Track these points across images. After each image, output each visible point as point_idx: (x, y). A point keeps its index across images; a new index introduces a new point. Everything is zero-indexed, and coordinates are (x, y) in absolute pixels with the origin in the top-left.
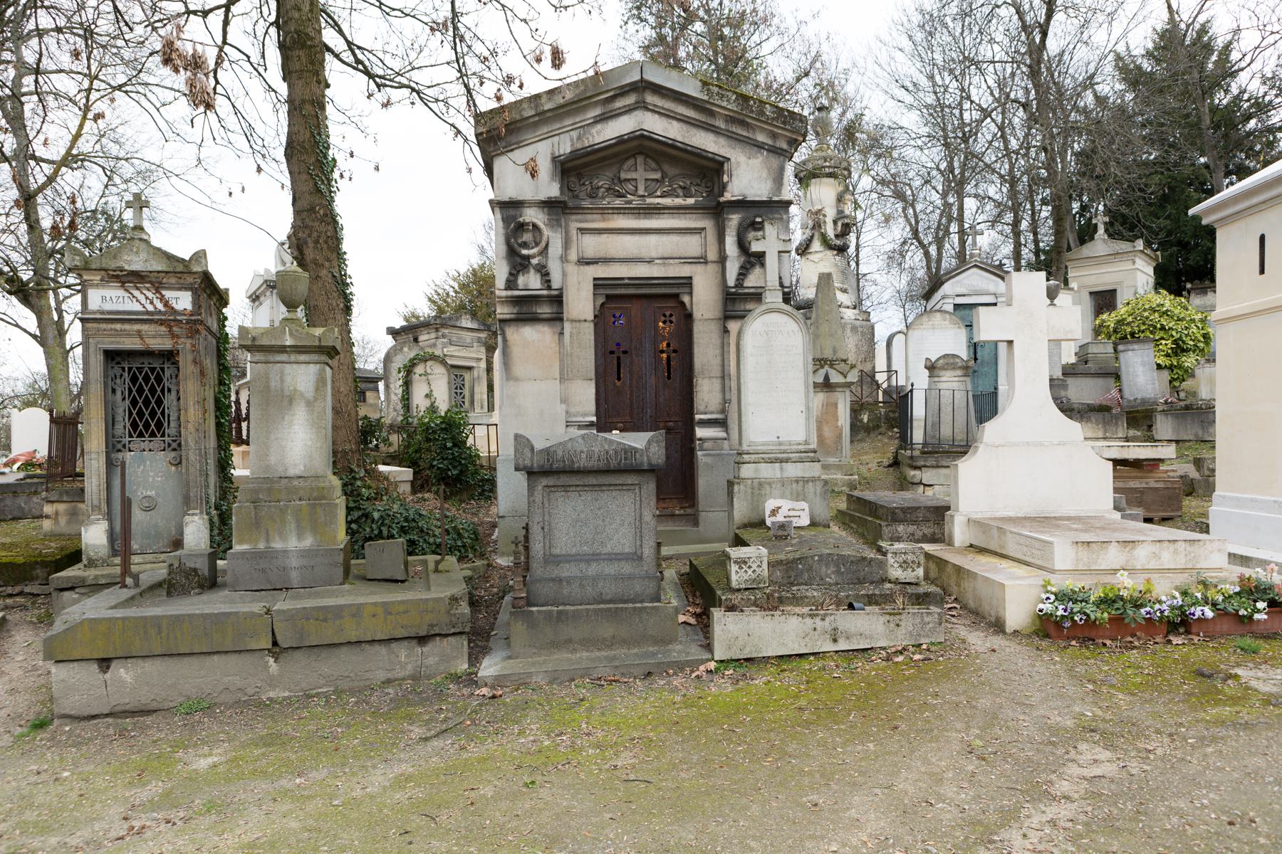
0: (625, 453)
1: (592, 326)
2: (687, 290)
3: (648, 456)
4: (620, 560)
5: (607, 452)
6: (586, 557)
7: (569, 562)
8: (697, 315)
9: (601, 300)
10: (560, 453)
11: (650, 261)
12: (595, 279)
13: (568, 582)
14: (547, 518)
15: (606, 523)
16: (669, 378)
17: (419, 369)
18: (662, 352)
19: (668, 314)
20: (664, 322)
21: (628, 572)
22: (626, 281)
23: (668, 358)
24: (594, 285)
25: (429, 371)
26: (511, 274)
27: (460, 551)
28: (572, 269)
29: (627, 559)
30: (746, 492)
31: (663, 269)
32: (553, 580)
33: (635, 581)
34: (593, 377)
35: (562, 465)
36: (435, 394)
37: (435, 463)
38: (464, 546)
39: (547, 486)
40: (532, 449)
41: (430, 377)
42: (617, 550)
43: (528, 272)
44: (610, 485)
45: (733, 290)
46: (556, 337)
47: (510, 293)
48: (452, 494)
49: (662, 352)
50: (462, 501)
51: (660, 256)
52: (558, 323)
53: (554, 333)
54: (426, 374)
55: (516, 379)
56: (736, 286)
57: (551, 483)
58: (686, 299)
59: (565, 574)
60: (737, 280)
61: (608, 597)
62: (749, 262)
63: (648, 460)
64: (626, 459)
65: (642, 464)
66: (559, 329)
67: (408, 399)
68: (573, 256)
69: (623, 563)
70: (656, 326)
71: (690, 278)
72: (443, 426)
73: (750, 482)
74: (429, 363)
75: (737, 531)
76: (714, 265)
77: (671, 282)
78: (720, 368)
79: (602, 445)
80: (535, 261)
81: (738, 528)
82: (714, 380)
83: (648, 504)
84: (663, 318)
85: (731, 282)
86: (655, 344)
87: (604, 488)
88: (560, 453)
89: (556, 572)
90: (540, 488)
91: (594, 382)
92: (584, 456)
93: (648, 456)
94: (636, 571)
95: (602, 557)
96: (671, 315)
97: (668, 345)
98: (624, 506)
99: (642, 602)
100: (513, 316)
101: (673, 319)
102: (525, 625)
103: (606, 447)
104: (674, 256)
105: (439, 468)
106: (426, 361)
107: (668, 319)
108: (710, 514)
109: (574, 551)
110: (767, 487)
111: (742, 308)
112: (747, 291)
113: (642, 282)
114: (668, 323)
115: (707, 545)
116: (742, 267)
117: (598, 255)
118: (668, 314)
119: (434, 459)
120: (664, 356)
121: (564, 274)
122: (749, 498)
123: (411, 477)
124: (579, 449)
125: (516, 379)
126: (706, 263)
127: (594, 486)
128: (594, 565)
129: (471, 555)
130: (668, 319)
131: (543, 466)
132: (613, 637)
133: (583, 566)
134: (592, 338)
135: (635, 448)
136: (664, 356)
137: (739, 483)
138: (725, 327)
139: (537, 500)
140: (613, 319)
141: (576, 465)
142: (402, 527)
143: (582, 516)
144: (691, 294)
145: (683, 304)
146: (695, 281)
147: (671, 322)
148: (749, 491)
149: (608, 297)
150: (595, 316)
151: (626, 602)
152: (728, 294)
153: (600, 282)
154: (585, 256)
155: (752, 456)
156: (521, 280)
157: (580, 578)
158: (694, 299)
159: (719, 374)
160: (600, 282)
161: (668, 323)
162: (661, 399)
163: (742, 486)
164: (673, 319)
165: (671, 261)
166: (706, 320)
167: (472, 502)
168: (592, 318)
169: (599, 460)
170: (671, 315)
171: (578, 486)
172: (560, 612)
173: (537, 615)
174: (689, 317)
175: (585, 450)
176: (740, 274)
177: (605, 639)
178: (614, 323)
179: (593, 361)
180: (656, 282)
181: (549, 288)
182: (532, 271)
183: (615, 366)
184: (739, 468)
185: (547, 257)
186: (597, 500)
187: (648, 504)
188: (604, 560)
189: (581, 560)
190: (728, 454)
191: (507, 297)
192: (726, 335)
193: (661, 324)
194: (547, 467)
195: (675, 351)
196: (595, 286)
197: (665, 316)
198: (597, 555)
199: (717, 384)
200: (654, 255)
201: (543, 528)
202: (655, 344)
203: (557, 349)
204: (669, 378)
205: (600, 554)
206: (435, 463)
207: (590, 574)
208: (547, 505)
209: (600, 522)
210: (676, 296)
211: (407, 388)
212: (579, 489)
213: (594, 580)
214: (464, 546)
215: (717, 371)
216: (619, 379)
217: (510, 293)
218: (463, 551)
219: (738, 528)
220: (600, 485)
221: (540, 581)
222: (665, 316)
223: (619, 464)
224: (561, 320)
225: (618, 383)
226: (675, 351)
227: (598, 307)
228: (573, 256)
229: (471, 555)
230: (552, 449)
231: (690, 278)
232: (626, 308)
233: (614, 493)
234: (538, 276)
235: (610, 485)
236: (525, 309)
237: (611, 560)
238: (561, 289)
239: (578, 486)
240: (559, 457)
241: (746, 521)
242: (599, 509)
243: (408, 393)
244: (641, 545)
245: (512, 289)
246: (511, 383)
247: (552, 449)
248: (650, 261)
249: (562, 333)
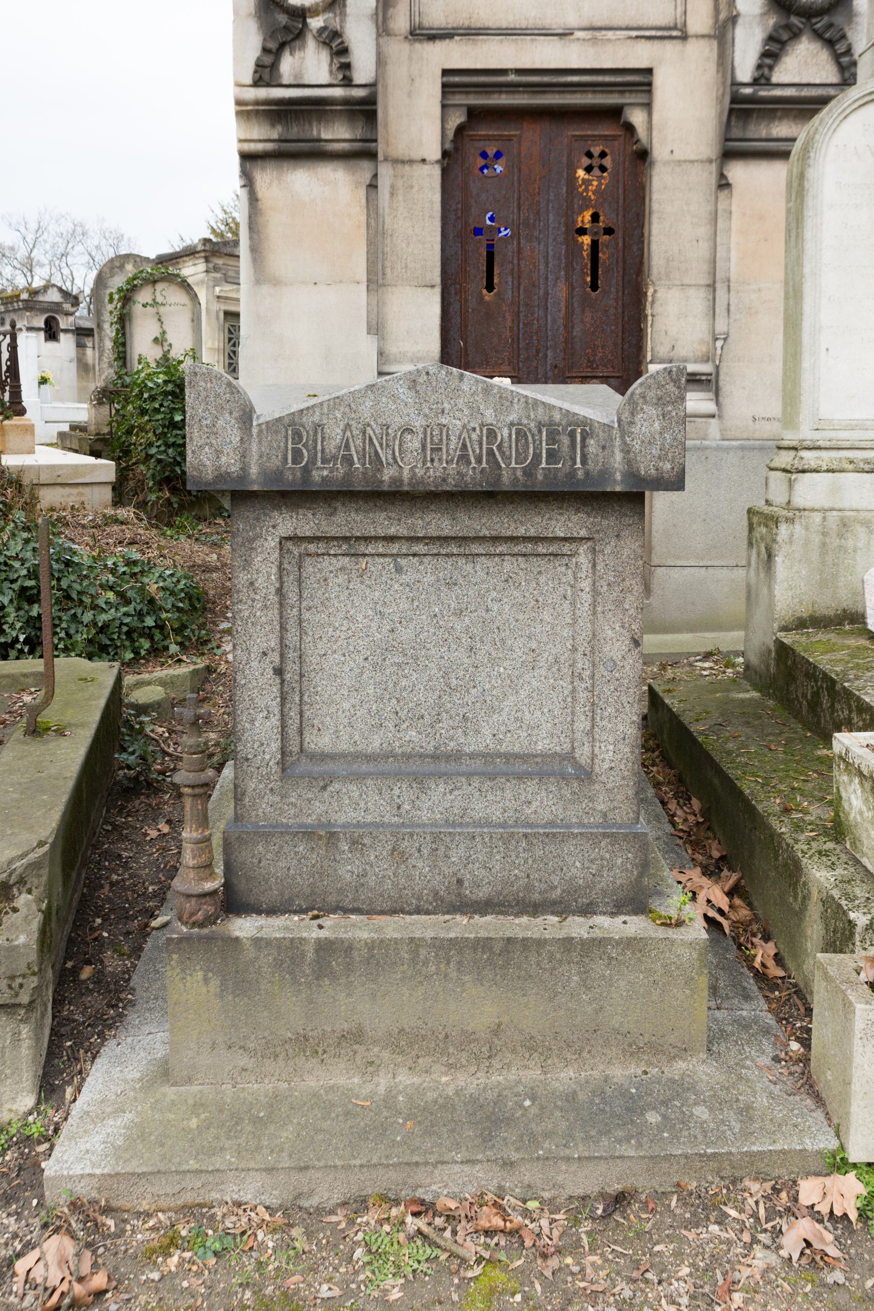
0: (553, 437)
1: (437, 172)
2: (641, 98)
3: (626, 450)
4: (520, 777)
5: (492, 434)
6: (414, 766)
7: (359, 777)
8: (659, 152)
9: (457, 119)
10: (335, 434)
11: (565, 34)
12: (446, 72)
13: (355, 843)
14: (292, 637)
15: (481, 656)
16: (594, 286)
17: (144, 296)
18: (582, 231)
19: (596, 151)
20: (589, 169)
21: (546, 816)
22: (512, 78)
23: (595, 244)
24: (444, 86)
25: (160, 299)
26: (265, 50)
27: (151, 637)
28: (398, 49)
29: (542, 776)
30: (807, 542)
31: (591, 50)
32: (308, 834)
33: (569, 847)
34: (437, 280)
35: (341, 470)
36: (171, 337)
37: (153, 451)
38: (160, 626)
39: (295, 539)
40: (246, 415)
41: (162, 309)
42: (513, 744)
43: (303, 47)
44: (496, 539)
45: (748, 91)
46: (362, 192)
47: (263, 93)
48: (182, 507)
49: (582, 231)
50: (200, 519)
51: (585, 23)
52: (366, 166)
53: (357, 185)
54: (155, 303)
55: (276, 282)
56: (756, 82)
57: (307, 530)
58: (637, 118)
59: (346, 815)
60: (759, 67)
61: (482, 894)
62: (788, 27)
63: (629, 462)
64: (552, 456)
65: (605, 473)
66: (367, 177)
67: (124, 344)
68: (401, 22)
69: (532, 785)
70: (572, 179)
71: (649, 71)
72: (170, 387)
73: (817, 518)
74: (160, 286)
75: (788, 639)
76: (703, 43)
77: (608, 79)
78: (705, 267)
79: (475, 411)
80: (315, 23)
81: (785, 629)
82: (692, 292)
83: (619, 603)
84: (586, 161)
85: (745, 71)
86: (570, 212)
87: (476, 548)
88: (335, 434)
89: (318, 808)
90: (272, 543)
91: (438, 290)
92: (413, 443)
93: (626, 450)
94: (573, 814)
95: (467, 765)
96: (603, 155)
97: (595, 218)
98: (538, 606)
99: (587, 911)
100: (270, 146)
101: (607, 162)
102: (215, 983)
103: (489, 416)
104: (615, 23)
105: (159, 461)
106: (155, 282)
107: (596, 162)
108: (675, 573)
109: (375, 744)
110: (861, 531)
111: (764, 134)
112: (778, 92)
113: (546, 79)
114: (596, 172)
115: (668, 637)
116: (771, 39)
117: (452, 21)
118: (596, 151)
119: (151, 445)
120: (586, 240)
121: (381, 61)
122: (815, 556)
123: (112, 477)
124: (397, 422)
125: (276, 282)
126: (684, 37)
127: (445, 540)
128: (438, 790)
129: (174, 648)
130: (596, 162)
131: (278, 474)
132: (497, 1030)
133: (403, 792)
134: (437, 197)
135: (585, 422)
136: (586, 240)
137: (790, 521)
138: (722, 176)
139: (260, 582)
140: (481, 162)
141: (387, 474)
142: (23, 589)
143: (405, 634)
144: (648, 106)
145: (630, 128)
146: (659, 80)
147: (603, 169)
148: (816, 539)
149: (475, 114)
150: (445, 154)
151: (535, 909)
152: (736, 99)
153: (457, 79)
154: (426, 24)
155: (824, 454)
156: (287, 65)
157: (395, 830)
158: (656, 117)
159: (704, 280)
160: (457, 79)
161: (596, 172)
162: (577, 331)
163: (798, 528)
164: (607, 162)
165: (610, 34)
166: (680, 162)
167: (219, 521)
168: (438, 155)
169: (464, 458)
170: (603, 155)
171: (392, 539)
172: (325, 947)
173: (250, 952)
174: (643, 156)
175: (418, 423)
176: (765, 54)
177: (469, 1037)
178: (482, 169)
179: (438, 247)
180: (575, 79)
181: (347, 82)
182: (311, 44)
183: (483, 260)
184: (791, 484)
185: (343, 15)
186: (451, 584)
187: (619, 603)
188: (469, 775)
189: (398, 776)
190: (718, 448)
191: (257, 103)
192: (723, 194)
193: (581, 173)
194: (292, 478)
195: (609, 231)
196: (447, 88)
197: (589, 155)
198: (449, 757)
199: (698, 300)
200: (572, 20)
201: (279, 672)
202: (570, 212)
203: (363, 218)
204: (594, 286)
205: (456, 756)
206: (153, 451)
207: (425, 816)
208: (292, 597)
209: (461, 655)
210: (615, 113)
211: (123, 328)
212: (395, 548)
213: (436, 838)
214: (160, 626)
215: (699, 274)
216: (490, 287)
217: (263, 93)
218: (158, 636)
219: (785, 629)
220: (463, 540)
221: (265, 835)
222: (589, 155)
223: (529, 472)
224: (371, 155)
225: (488, 296)
226: (609, 231)
227: (450, 134)
228: (401, 22)
229: (174, 648)
230: (308, 420)
231: (649, 71)
232: (509, 139)
233: (508, 565)
234: (324, 56)
235: (496, 539)
236: (295, 132)
237: (492, 777)
238: (373, 85)
239: (392, 539)
240: (331, 447)
241: (804, 611)
242: (459, 613)
243: (124, 334)
244: (590, 733)
245: (269, 85)
246: (265, 289)
247: (308, 420)
248: (565, 34)
249: (373, 186)
